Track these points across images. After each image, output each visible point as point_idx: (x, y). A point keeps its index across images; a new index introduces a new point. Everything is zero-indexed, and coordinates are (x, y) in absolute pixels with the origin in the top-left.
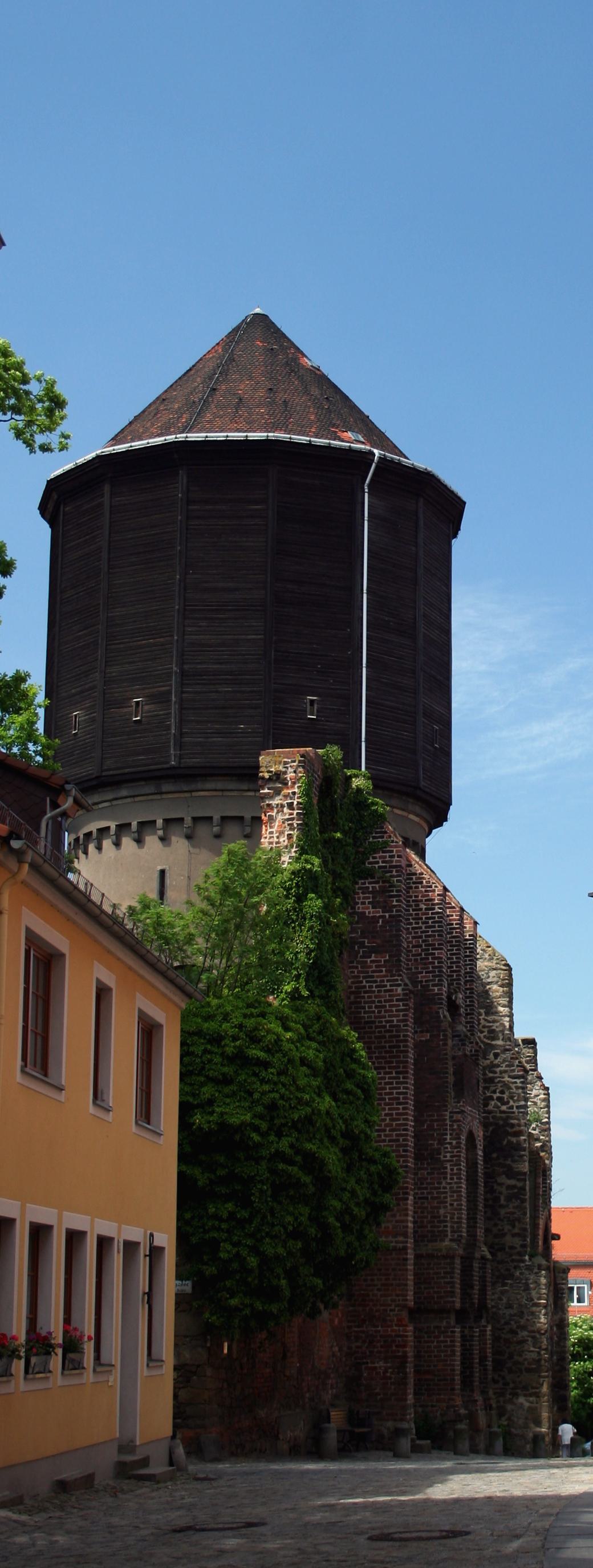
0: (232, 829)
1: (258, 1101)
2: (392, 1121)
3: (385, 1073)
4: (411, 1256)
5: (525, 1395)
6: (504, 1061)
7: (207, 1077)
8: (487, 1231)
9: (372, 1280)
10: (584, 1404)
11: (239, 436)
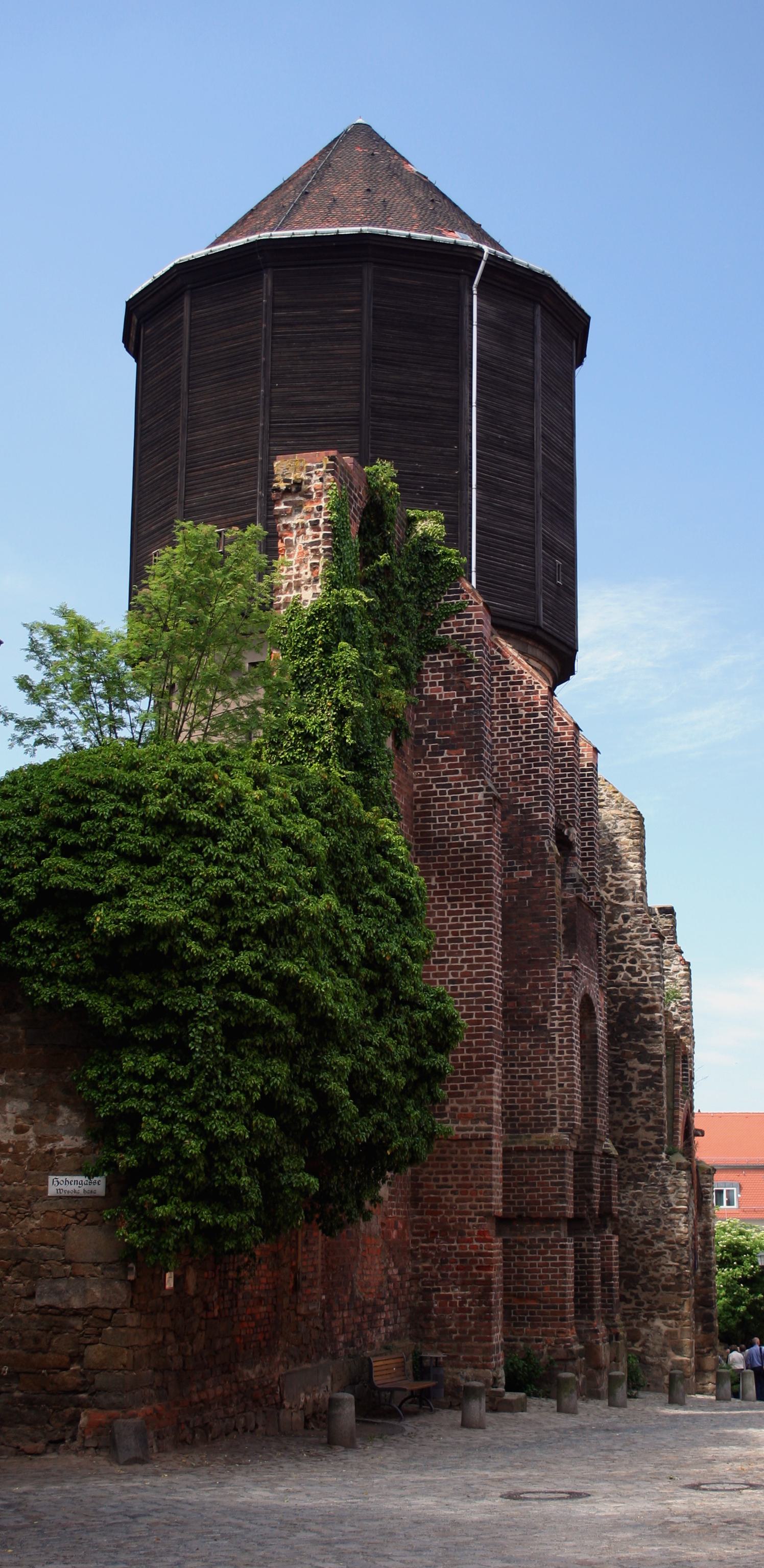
1: (200, 891)
2: (461, 963)
3: (462, 906)
4: (497, 1147)
5: (663, 1317)
6: (635, 924)
7: (118, 852)
9: (446, 1180)
10: (734, 1313)
11: (330, 231)
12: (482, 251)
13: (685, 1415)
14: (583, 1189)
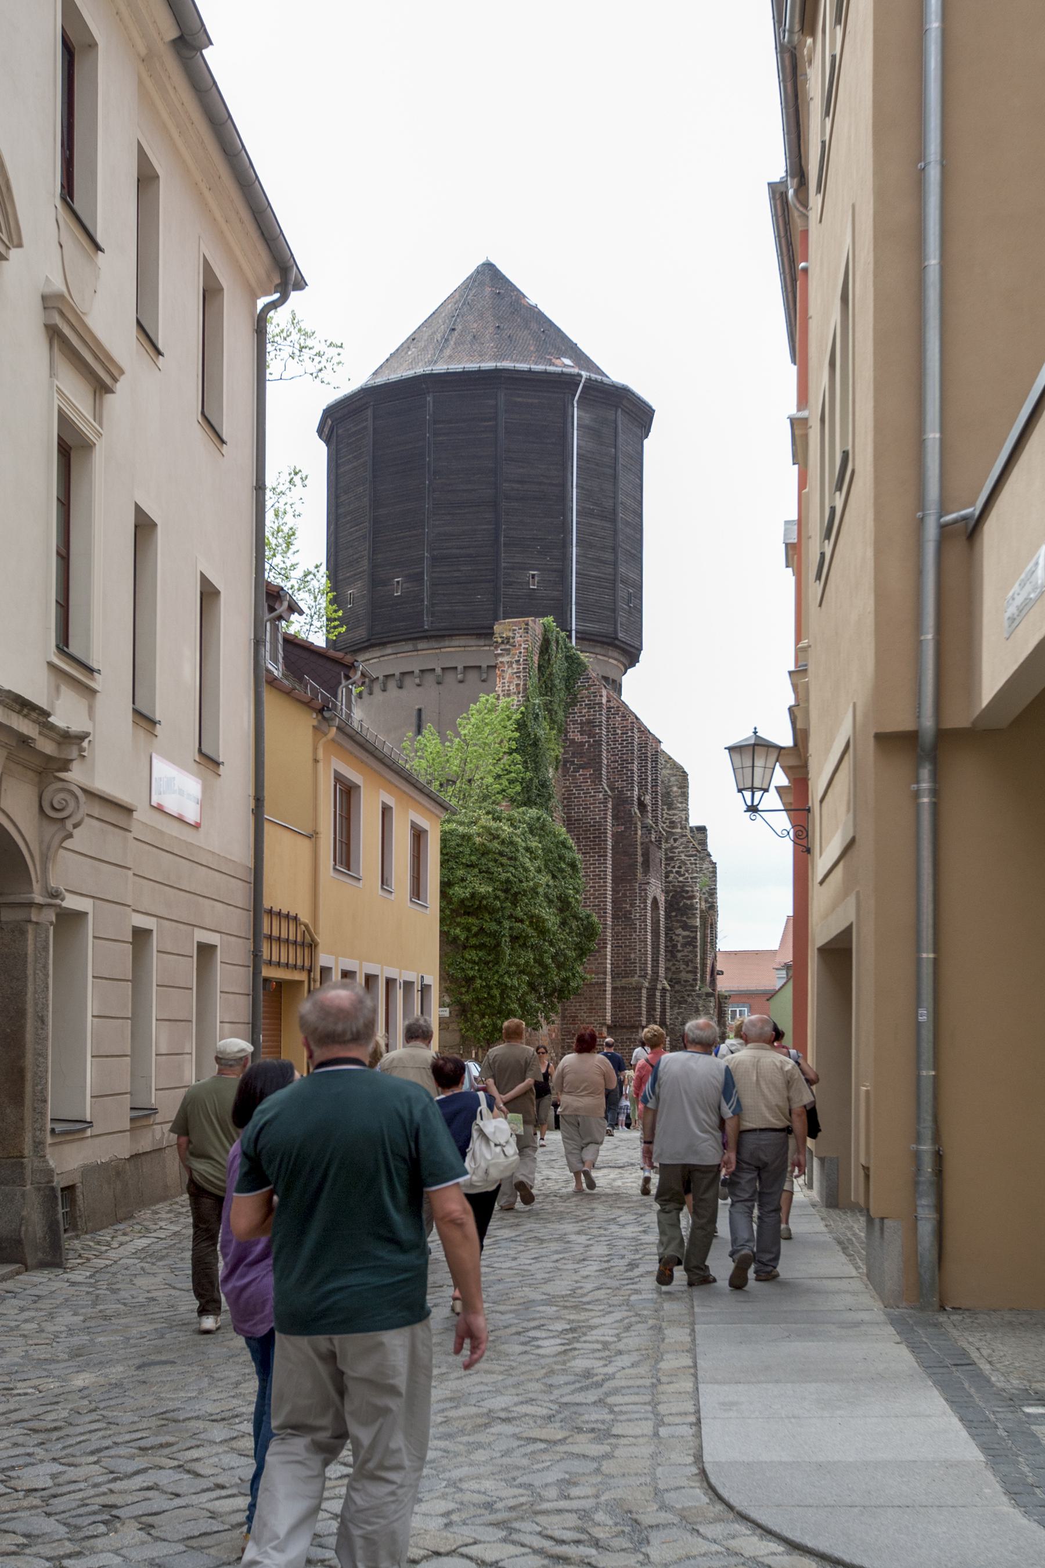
0: (472, 676)
4: (609, 988)
8: (667, 969)
12: (581, 376)
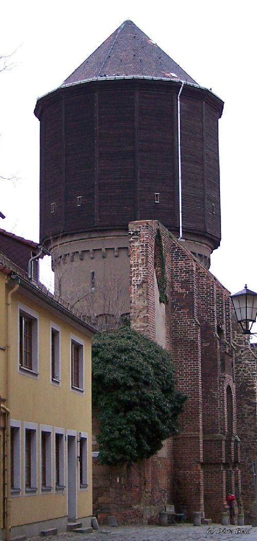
4: (201, 440)
12: (182, 83)
13: (181, 155)
14: (228, 453)
